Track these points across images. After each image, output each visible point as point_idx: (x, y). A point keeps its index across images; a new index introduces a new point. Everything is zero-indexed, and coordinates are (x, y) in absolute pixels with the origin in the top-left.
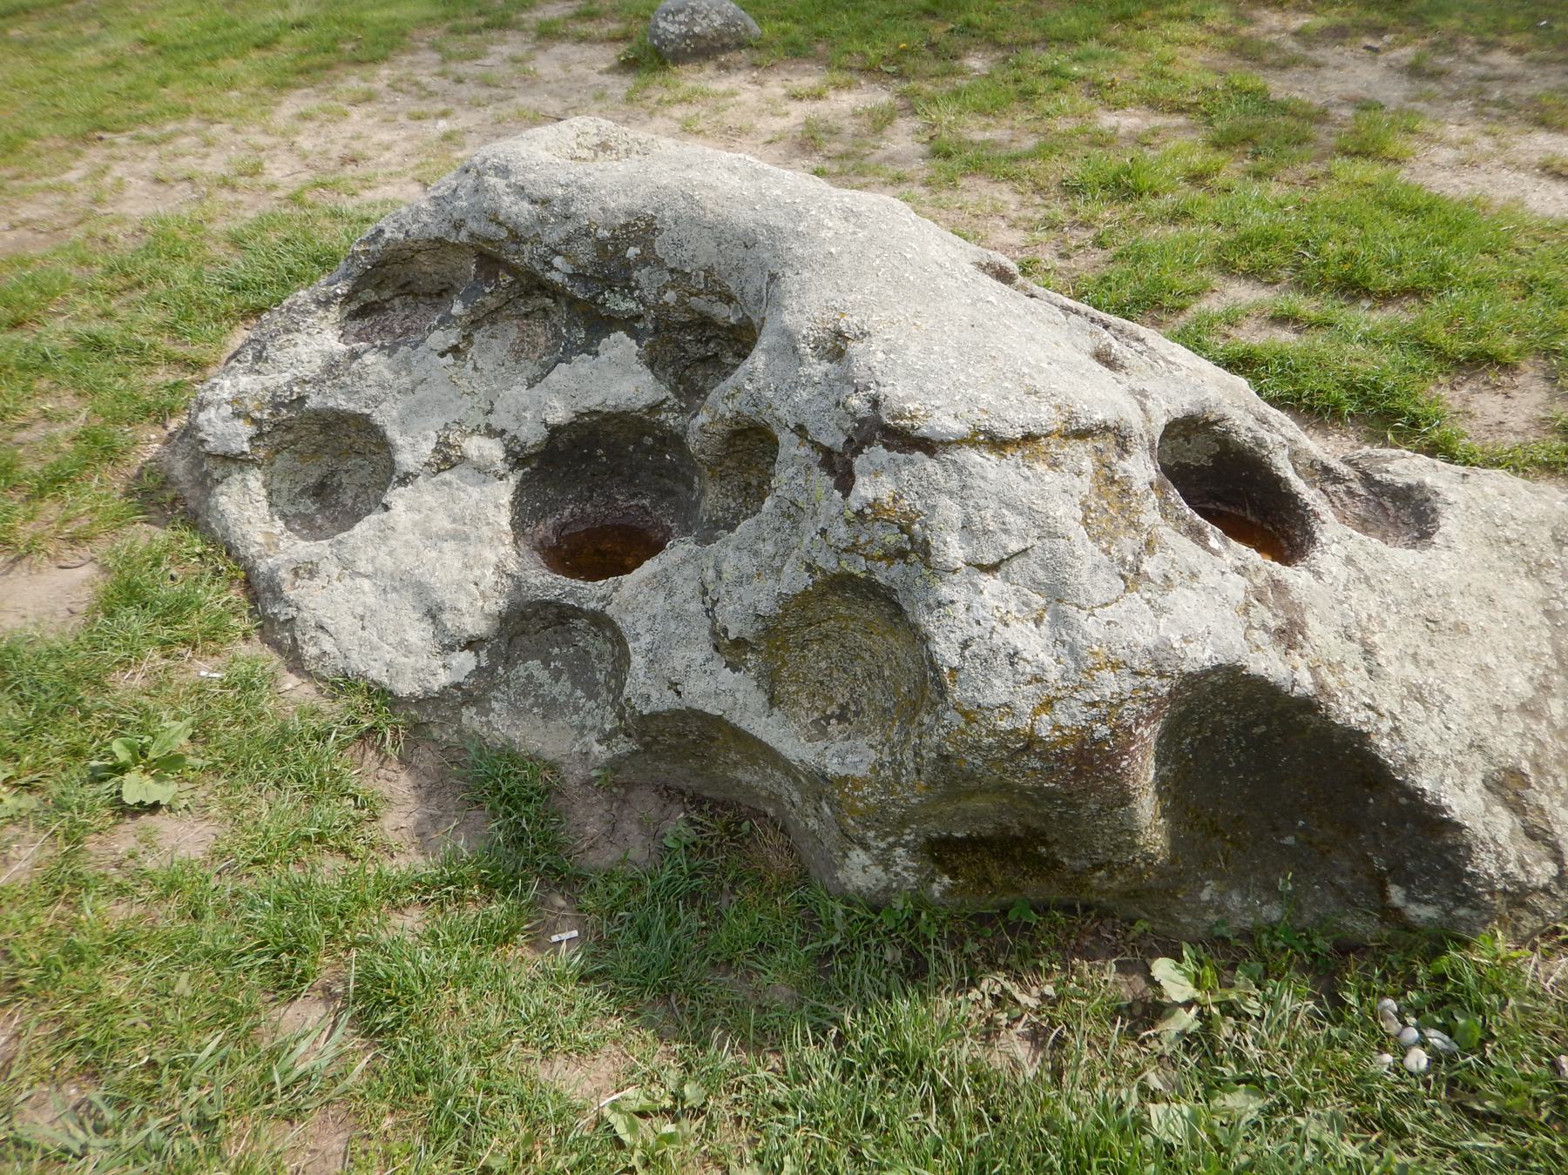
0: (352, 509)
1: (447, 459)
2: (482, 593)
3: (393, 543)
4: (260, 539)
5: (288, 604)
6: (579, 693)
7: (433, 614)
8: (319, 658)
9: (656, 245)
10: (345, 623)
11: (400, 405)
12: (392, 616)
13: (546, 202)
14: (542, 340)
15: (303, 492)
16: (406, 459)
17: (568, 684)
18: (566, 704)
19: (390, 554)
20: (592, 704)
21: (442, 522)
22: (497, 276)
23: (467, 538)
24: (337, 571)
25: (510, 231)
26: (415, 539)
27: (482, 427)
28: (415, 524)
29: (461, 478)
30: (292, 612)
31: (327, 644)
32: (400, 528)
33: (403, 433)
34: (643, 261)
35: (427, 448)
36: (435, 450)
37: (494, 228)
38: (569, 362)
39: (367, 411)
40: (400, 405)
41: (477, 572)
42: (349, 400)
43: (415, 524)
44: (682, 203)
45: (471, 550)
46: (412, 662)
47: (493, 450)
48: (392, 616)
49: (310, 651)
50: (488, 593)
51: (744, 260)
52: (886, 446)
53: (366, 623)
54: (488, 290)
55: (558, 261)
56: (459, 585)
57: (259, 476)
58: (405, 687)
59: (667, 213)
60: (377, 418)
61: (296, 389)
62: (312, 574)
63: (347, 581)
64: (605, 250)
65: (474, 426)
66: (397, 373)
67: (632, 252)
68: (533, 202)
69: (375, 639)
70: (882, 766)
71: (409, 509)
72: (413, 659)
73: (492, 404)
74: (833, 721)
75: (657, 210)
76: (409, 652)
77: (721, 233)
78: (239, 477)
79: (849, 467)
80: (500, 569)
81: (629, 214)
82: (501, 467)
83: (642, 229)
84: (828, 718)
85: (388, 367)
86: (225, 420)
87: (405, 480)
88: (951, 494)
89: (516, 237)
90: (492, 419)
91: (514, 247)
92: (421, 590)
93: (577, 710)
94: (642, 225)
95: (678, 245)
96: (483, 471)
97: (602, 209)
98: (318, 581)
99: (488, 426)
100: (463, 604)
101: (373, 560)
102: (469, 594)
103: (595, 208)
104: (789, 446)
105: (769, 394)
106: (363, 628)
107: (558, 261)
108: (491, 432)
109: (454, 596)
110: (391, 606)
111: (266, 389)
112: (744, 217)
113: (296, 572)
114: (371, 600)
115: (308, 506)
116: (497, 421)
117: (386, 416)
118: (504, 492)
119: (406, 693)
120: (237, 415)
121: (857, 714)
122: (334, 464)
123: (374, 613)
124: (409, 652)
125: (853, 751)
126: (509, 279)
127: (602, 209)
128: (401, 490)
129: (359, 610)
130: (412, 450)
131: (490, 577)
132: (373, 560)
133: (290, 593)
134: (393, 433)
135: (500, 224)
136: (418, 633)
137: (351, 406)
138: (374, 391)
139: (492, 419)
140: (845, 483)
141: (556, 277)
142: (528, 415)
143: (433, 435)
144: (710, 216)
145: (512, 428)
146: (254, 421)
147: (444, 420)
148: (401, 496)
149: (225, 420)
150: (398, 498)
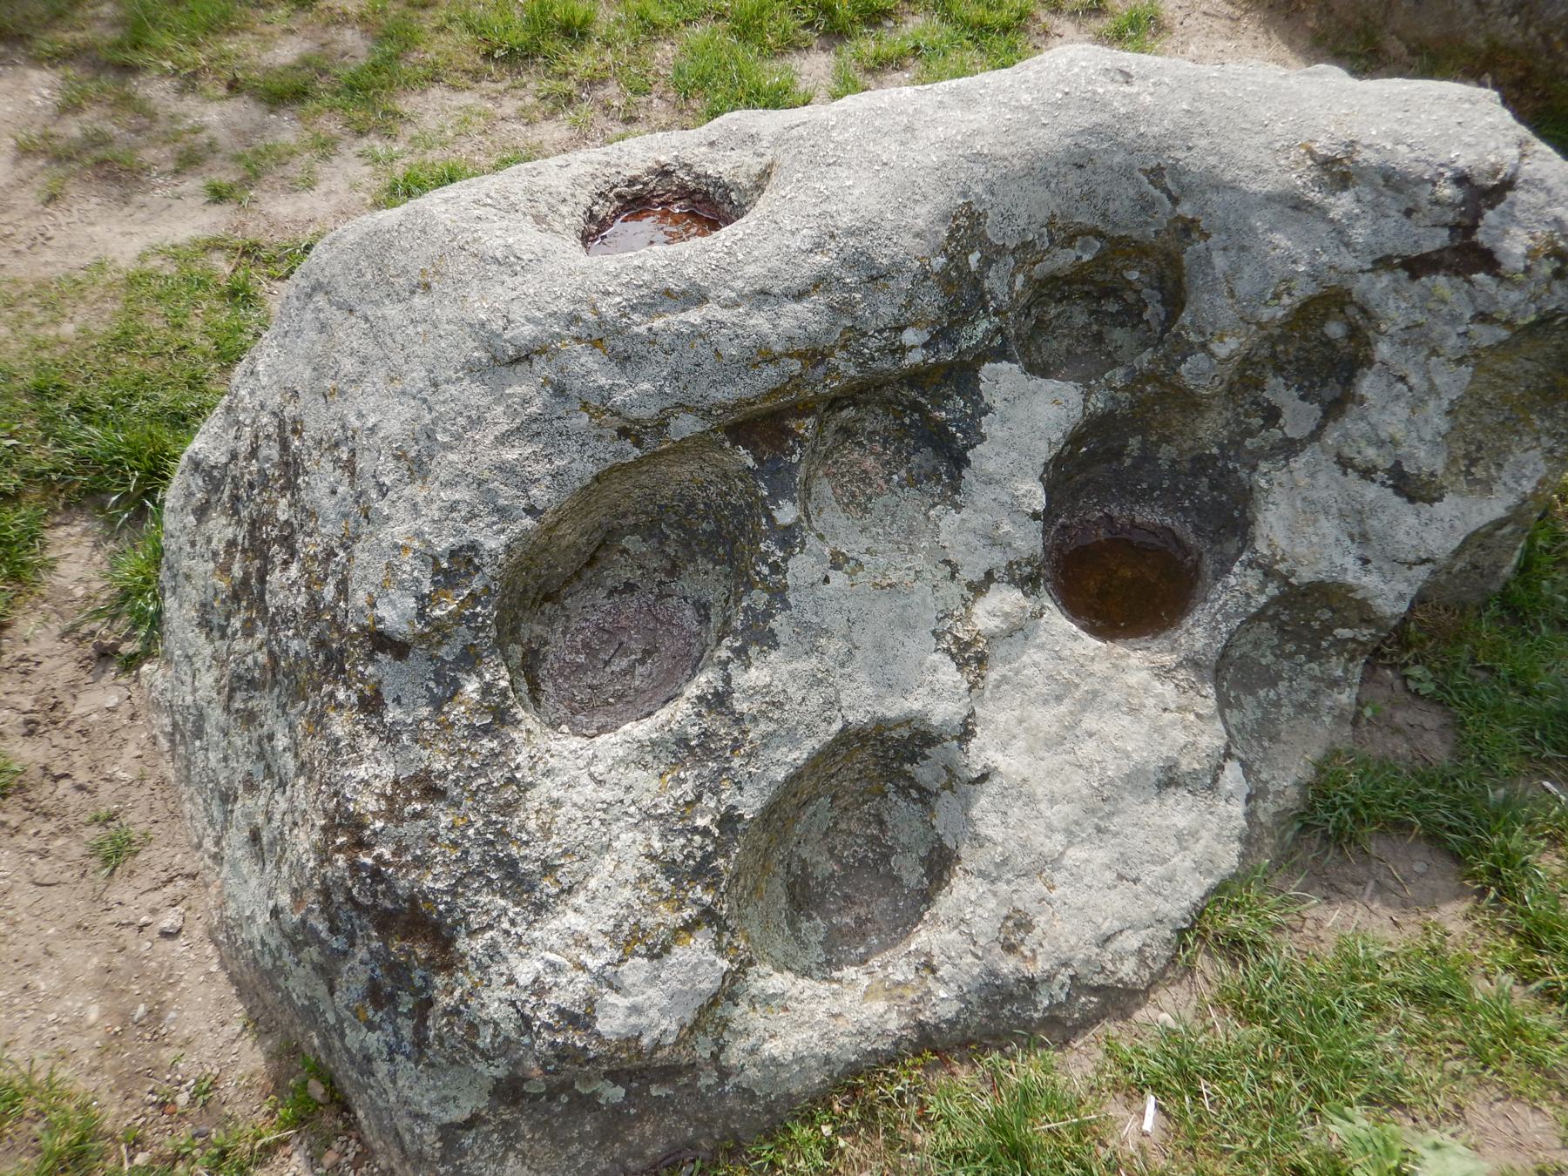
0: (844, 867)
1: (971, 657)
2: (1180, 709)
3: (1040, 791)
4: (880, 1006)
5: (1049, 978)
6: (1262, 693)
7: (1170, 779)
8: (1143, 962)
9: (989, 234)
10: (1113, 905)
11: (861, 676)
12: (1141, 835)
13: (821, 282)
14: (870, 462)
15: (792, 924)
16: (944, 713)
17: (1250, 698)
18: (1266, 712)
19: (1053, 801)
20: (1282, 686)
21: (1046, 718)
22: (790, 433)
23: (1095, 693)
24: (1039, 885)
25: (800, 355)
26: (1052, 760)
27: (966, 592)
28: (1030, 750)
29: (1006, 660)
30: (1064, 976)
31: (1132, 941)
32: (1027, 773)
33: (905, 692)
34: (987, 262)
35: (949, 674)
36: (960, 667)
37: (770, 371)
38: (983, 438)
39: (837, 726)
40: (861, 676)
41: (1150, 702)
42: (795, 743)
43: (1030, 750)
44: (979, 170)
45: (1113, 696)
46: (1197, 842)
47: (1005, 600)
48: (1141, 835)
49: (1128, 970)
50: (1183, 701)
51: (1087, 182)
52: (1492, 207)
53: (1133, 875)
54: (795, 459)
55: (910, 337)
56: (1158, 729)
57: (766, 968)
58: (1229, 859)
59: (979, 189)
60: (857, 717)
61: (701, 822)
62: (1024, 924)
63: (1058, 877)
64: (950, 282)
65: (958, 601)
66: (814, 649)
67: (974, 259)
68: (799, 296)
69: (1159, 870)
70: (1551, 451)
71: (1004, 747)
72: (1204, 833)
73: (947, 562)
74: (1473, 470)
75: (964, 194)
76: (1194, 834)
77: (1040, 171)
78: (744, 1006)
79: (1475, 248)
80: (1163, 673)
81: (944, 219)
82: (1028, 604)
83: (966, 227)
84: (1468, 473)
85: (794, 657)
86: (652, 980)
87: (966, 733)
88: (1549, 204)
89: (814, 356)
90: (965, 575)
91: (821, 370)
92: (1134, 780)
93: (1277, 704)
94: (962, 221)
95: (1008, 217)
96: (1018, 630)
97: (917, 235)
98: (1041, 921)
99: (970, 586)
100: (1181, 737)
101: (1051, 829)
102: (1173, 724)
103: (908, 240)
104: (1377, 288)
105: (1325, 258)
106: (1136, 881)
107: (910, 337)
108: (979, 588)
109: (1168, 742)
110: (1129, 830)
111: (643, 879)
112: (1047, 139)
113: (1010, 948)
114: (1101, 856)
115: (814, 928)
116: (972, 572)
117: (861, 702)
118: (1057, 622)
119: (1235, 862)
120: (657, 954)
121: (1479, 448)
122: (874, 816)
123: (1124, 859)
124: (1194, 834)
125: (1520, 465)
126: (810, 421)
127: (917, 235)
128: (974, 743)
129: (1109, 876)
130: (936, 693)
131: (1167, 690)
132: (1051, 829)
133: (1038, 969)
134: (895, 707)
135: (773, 359)
136: (1179, 811)
137: (810, 745)
138: (815, 699)
139: (965, 575)
140: (1488, 261)
141: (915, 357)
142: (1006, 527)
143: (936, 657)
144: (1015, 161)
145: (998, 559)
146: (690, 927)
147: (925, 633)
148: (981, 749)
149: (652, 980)
150: (982, 752)
